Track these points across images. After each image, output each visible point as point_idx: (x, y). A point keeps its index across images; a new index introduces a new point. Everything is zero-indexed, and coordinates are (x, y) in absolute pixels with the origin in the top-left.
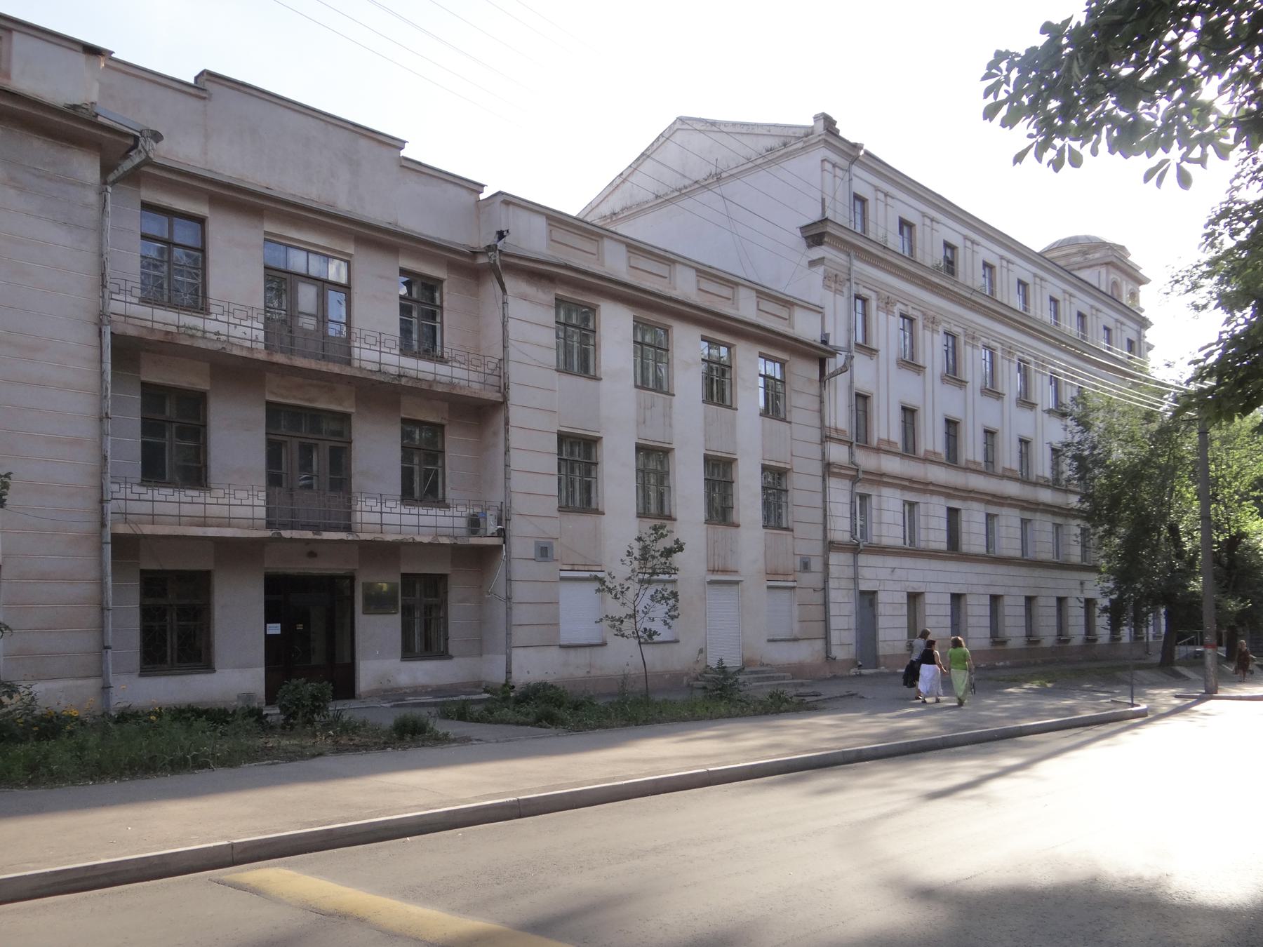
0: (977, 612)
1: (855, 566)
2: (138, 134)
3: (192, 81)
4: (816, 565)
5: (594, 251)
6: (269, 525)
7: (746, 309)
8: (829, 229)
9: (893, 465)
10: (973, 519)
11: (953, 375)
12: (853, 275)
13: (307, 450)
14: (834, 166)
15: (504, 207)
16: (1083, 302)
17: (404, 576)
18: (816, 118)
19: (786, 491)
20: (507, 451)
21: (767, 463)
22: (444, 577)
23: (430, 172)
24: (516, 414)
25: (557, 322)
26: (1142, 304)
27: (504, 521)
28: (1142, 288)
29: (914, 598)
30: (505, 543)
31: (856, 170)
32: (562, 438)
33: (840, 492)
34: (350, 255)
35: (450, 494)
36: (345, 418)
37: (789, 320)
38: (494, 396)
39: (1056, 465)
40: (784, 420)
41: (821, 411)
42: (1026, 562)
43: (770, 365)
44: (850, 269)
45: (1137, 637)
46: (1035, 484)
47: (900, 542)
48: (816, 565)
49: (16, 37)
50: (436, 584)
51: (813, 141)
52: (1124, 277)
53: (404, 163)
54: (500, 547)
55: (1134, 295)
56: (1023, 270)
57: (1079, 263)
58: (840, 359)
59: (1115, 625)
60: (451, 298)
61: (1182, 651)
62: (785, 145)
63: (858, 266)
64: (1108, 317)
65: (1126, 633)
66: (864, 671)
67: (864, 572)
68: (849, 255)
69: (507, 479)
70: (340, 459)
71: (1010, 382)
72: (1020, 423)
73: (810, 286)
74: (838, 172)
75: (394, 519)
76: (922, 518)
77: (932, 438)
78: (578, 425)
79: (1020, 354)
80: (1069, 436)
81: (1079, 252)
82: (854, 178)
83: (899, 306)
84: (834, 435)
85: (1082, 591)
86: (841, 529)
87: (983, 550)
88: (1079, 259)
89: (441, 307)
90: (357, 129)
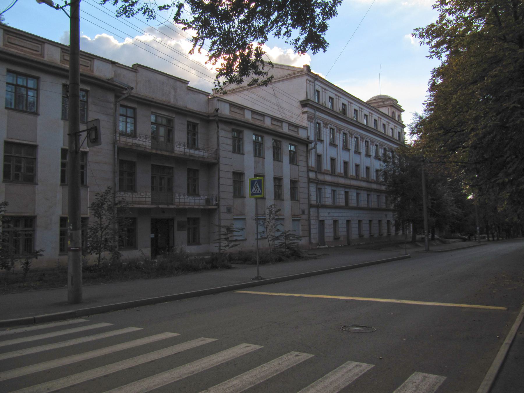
0: (354, 226)
1: (318, 213)
2: (127, 88)
3: (131, 66)
4: (306, 212)
5: (296, 131)
6: (152, 203)
7: (285, 129)
8: (309, 103)
9: (328, 178)
10: (353, 195)
11: (346, 148)
12: (316, 116)
13: (161, 179)
14: (310, 81)
15: (217, 101)
16: (384, 121)
17: (188, 218)
18: (304, 66)
19: (297, 188)
20: (219, 179)
21: (292, 179)
22: (198, 219)
23: (124, 67)
24: (222, 167)
25: (232, 137)
26: (402, 120)
27: (218, 201)
28: (402, 113)
29: (335, 222)
30: (218, 207)
31: (316, 82)
32: (234, 173)
33: (313, 188)
34: (174, 117)
35: (201, 192)
36: (171, 168)
37: (297, 132)
38: (215, 161)
39: (377, 177)
40: (296, 165)
41: (307, 161)
42: (368, 209)
43: (292, 147)
44: (315, 114)
45: (403, 233)
46: (371, 182)
47: (331, 204)
48: (306, 212)
49: (95, 60)
50: (196, 221)
51: (304, 73)
52: (396, 110)
53: (189, 88)
54: (216, 209)
55: (399, 116)
56: (366, 111)
57: (382, 105)
58: (313, 145)
59: (397, 229)
60: (201, 130)
61: (418, 237)
62: (294, 74)
63: (318, 113)
64: (392, 125)
65: (400, 233)
66: (321, 247)
67: (321, 214)
68: (315, 110)
69: (219, 187)
70: (170, 181)
71: (363, 150)
72: (366, 162)
73: (303, 121)
74: (311, 83)
75: (183, 201)
76: (337, 195)
77: (340, 169)
78: (238, 169)
79: (355, 135)
80: (381, 167)
81: (382, 101)
82: (316, 85)
83: (330, 125)
84: (311, 169)
85: (386, 218)
86: (314, 200)
87: (356, 205)
88: (382, 103)
89: (197, 132)
90: (177, 79)
